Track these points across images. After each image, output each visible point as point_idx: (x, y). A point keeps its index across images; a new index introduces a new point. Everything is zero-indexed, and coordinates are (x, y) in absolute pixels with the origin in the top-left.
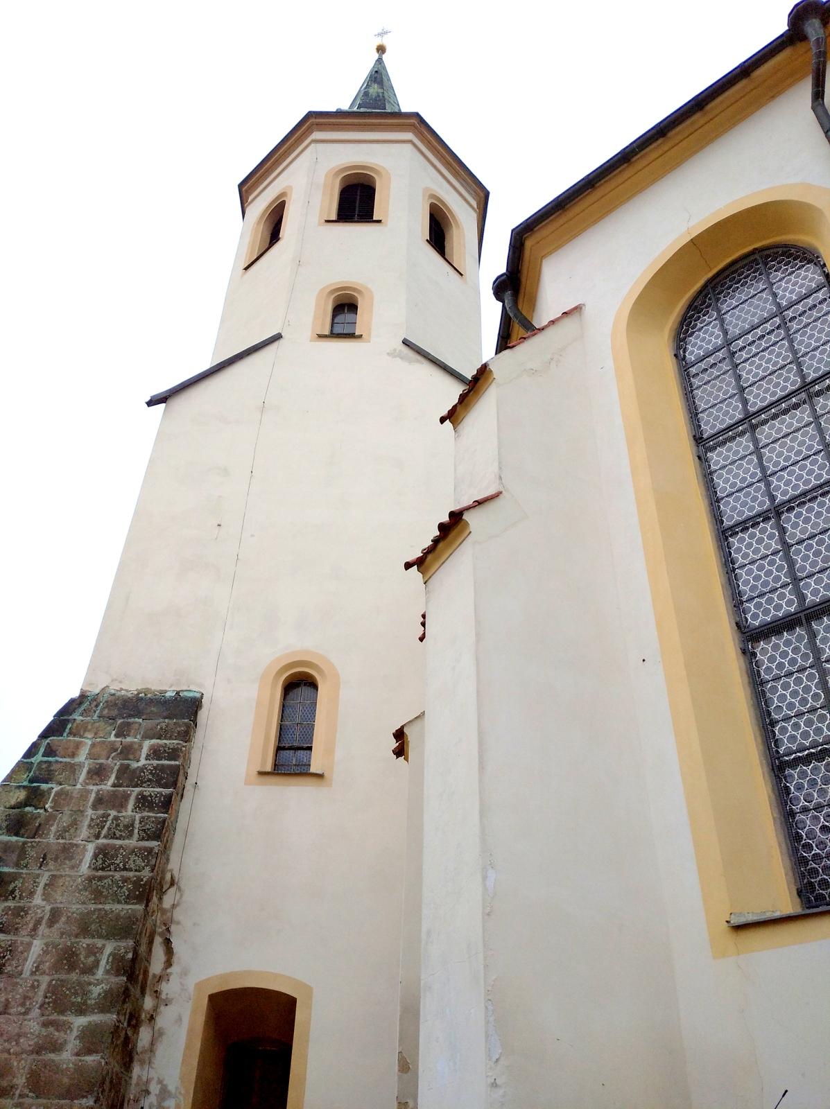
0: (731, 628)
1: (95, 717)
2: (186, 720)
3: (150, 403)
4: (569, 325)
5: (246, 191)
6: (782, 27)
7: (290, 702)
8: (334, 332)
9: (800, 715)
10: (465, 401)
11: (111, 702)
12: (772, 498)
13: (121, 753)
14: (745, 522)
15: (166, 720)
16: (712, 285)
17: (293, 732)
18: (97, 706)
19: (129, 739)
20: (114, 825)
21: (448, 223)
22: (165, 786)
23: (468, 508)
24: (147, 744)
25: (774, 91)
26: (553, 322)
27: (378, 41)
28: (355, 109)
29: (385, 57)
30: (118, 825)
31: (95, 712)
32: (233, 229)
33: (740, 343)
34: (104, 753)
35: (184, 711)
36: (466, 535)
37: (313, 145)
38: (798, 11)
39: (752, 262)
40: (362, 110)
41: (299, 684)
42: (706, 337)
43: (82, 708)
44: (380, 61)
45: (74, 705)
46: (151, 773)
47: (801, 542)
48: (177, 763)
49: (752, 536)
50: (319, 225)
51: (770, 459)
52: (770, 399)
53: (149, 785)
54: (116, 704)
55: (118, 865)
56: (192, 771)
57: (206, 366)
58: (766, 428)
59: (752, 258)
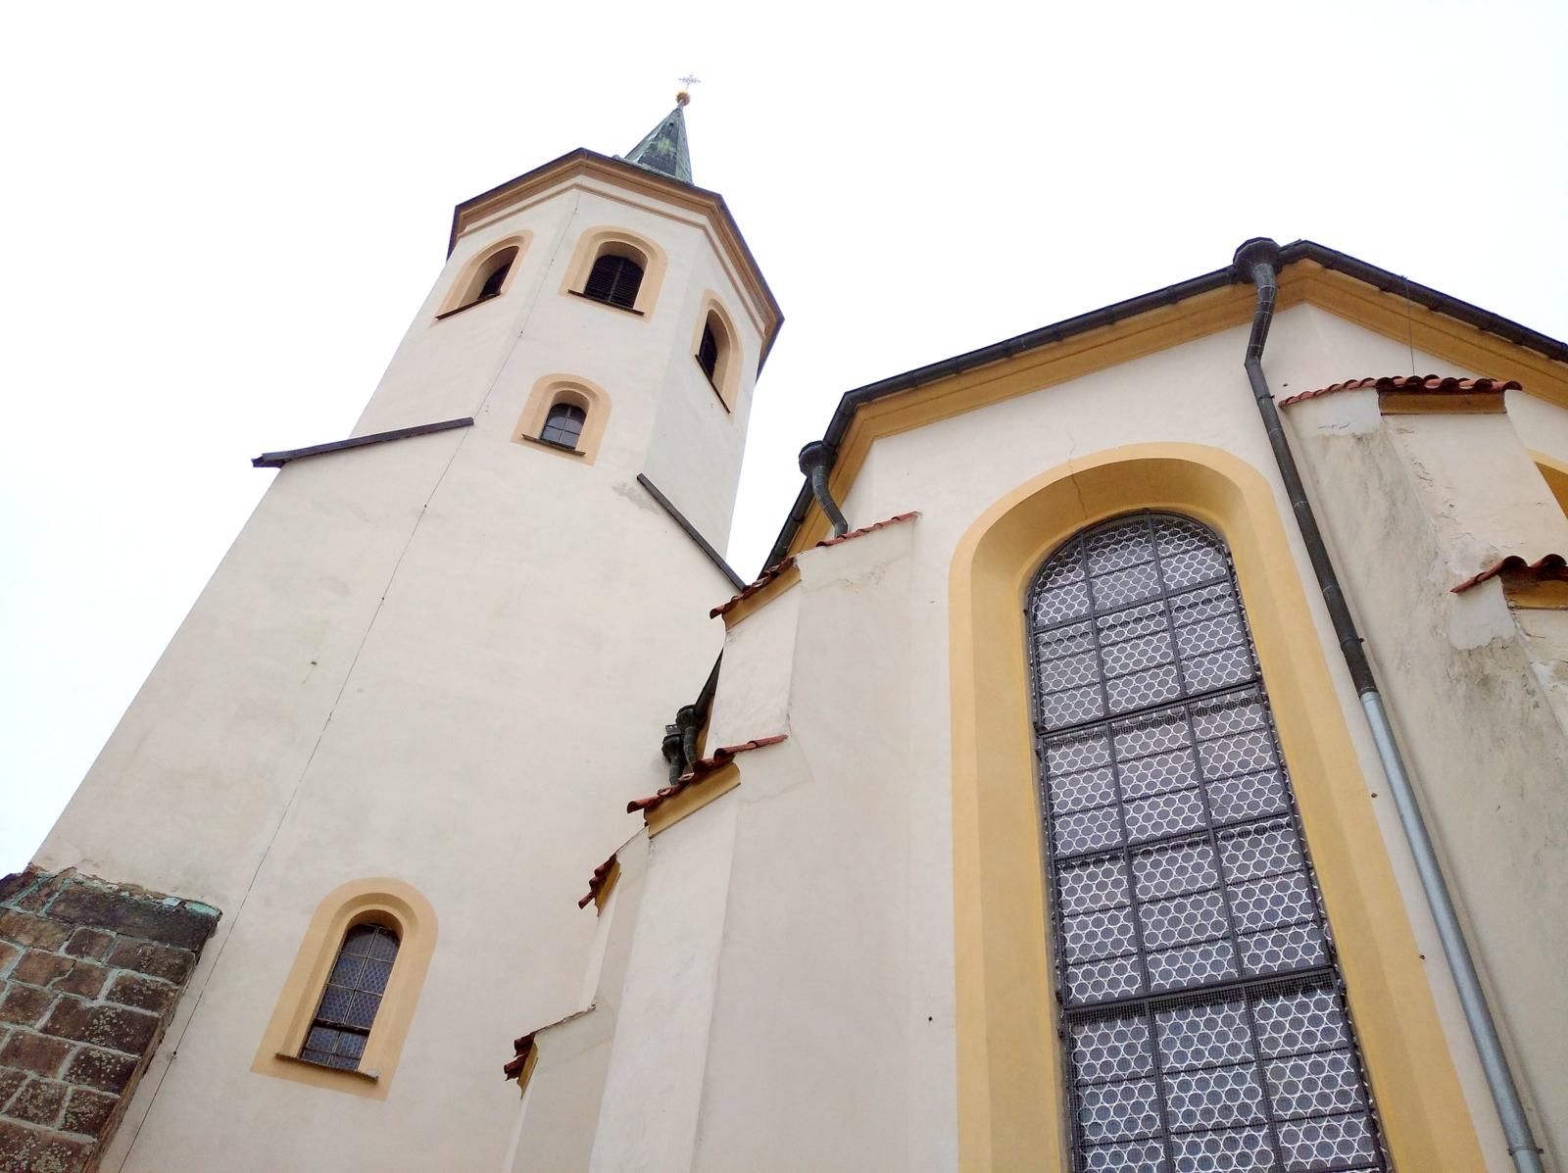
0: (1051, 997)
1: (42, 913)
2: (186, 950)
3: (259, 462)
4: (897, 532)
5: (465, 217)
6: (1225, 259)
8: (545, 438)
9: (1123, 1141)
10: (751, 597)
11: (73, 894)
12: (1125, 834)
13: (69, 979)
14: (1086, 855)
15: (155, 943)
16: (1087, 535)
17: (345, 1002)
18: (49, 895)
19: (88, 960)
20: (29, 1095)
21: (726, 342)
22: (128, 1049)
23: (741, 750)
24: (115, 974)
25: (1202, 328)
26: (880, 526)
27: (682, 88)
28: (635, 161)
29: (686, 110)
30: (34, 1097)
31: (44, 904)
32: (428, 265)
33: (1110, 620)
34: (42, 974)
35: (187, 932)
36: (731, 787)
37: (574, 190)
38: (1249, 248)
39: (1137, 523)
40: (645, 166)
41: (373, 931)
42: (1065, 600)
43: (24, 894)
44: (678, 112)
45: (13, 886)
46: (110, 1023)
47: (1154, 901)
48: (156, 1014)
49: (1092, 877)
50: (560, 293)
51: (1128, 781)
52: (1137, 703)
53: (101, 1041)
54: (79, 900)
55: (19, 1163)
56: (173, 1031)
57: (343, 435)
58: (1129, 737)
59: (1141, 518)
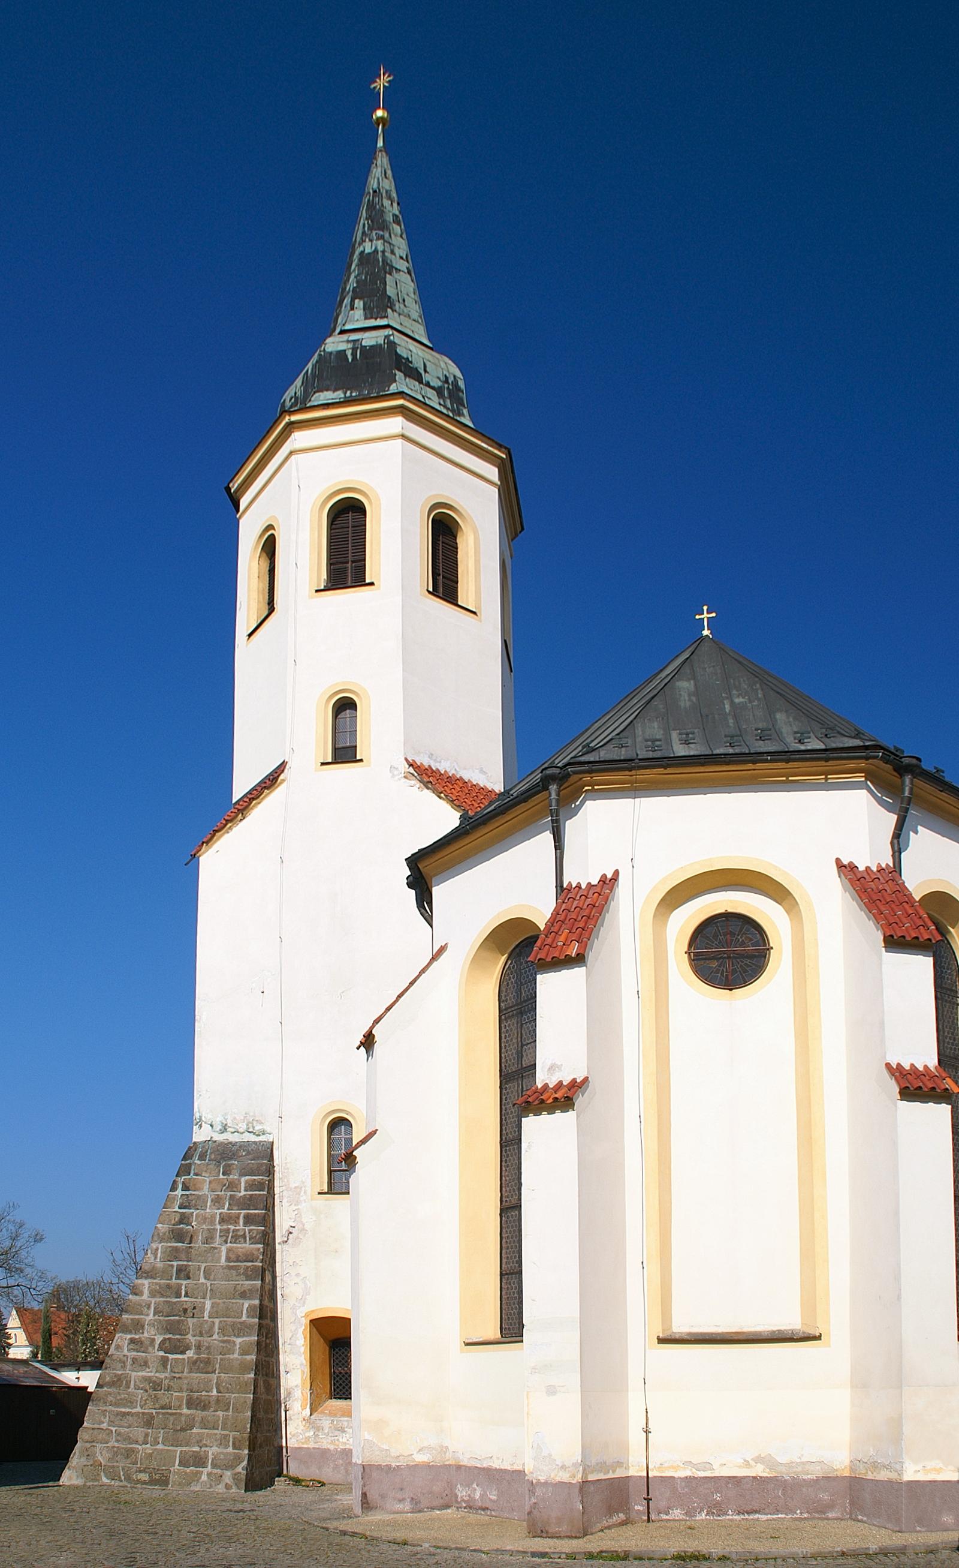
7: (339, 721)
24: (243, 1179)
